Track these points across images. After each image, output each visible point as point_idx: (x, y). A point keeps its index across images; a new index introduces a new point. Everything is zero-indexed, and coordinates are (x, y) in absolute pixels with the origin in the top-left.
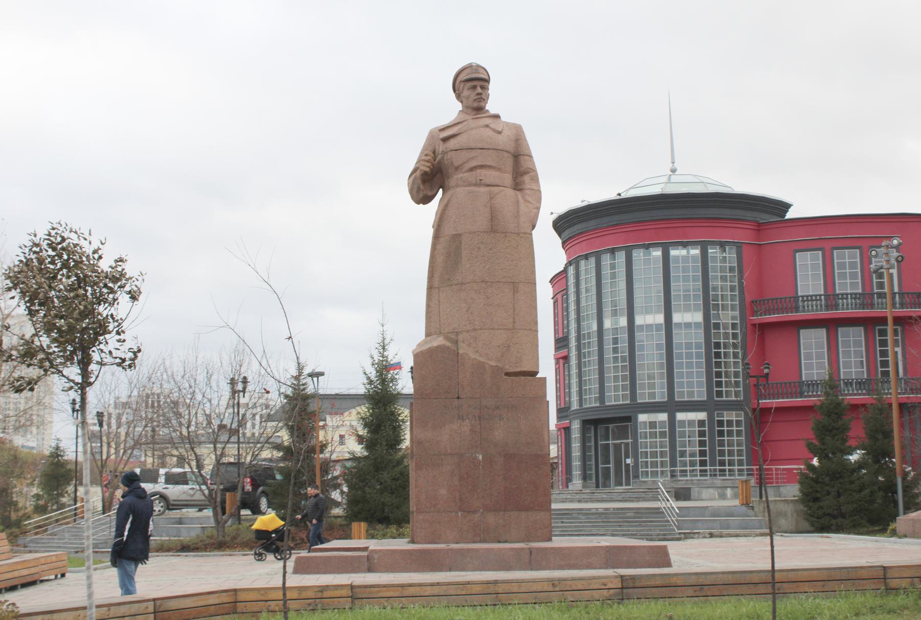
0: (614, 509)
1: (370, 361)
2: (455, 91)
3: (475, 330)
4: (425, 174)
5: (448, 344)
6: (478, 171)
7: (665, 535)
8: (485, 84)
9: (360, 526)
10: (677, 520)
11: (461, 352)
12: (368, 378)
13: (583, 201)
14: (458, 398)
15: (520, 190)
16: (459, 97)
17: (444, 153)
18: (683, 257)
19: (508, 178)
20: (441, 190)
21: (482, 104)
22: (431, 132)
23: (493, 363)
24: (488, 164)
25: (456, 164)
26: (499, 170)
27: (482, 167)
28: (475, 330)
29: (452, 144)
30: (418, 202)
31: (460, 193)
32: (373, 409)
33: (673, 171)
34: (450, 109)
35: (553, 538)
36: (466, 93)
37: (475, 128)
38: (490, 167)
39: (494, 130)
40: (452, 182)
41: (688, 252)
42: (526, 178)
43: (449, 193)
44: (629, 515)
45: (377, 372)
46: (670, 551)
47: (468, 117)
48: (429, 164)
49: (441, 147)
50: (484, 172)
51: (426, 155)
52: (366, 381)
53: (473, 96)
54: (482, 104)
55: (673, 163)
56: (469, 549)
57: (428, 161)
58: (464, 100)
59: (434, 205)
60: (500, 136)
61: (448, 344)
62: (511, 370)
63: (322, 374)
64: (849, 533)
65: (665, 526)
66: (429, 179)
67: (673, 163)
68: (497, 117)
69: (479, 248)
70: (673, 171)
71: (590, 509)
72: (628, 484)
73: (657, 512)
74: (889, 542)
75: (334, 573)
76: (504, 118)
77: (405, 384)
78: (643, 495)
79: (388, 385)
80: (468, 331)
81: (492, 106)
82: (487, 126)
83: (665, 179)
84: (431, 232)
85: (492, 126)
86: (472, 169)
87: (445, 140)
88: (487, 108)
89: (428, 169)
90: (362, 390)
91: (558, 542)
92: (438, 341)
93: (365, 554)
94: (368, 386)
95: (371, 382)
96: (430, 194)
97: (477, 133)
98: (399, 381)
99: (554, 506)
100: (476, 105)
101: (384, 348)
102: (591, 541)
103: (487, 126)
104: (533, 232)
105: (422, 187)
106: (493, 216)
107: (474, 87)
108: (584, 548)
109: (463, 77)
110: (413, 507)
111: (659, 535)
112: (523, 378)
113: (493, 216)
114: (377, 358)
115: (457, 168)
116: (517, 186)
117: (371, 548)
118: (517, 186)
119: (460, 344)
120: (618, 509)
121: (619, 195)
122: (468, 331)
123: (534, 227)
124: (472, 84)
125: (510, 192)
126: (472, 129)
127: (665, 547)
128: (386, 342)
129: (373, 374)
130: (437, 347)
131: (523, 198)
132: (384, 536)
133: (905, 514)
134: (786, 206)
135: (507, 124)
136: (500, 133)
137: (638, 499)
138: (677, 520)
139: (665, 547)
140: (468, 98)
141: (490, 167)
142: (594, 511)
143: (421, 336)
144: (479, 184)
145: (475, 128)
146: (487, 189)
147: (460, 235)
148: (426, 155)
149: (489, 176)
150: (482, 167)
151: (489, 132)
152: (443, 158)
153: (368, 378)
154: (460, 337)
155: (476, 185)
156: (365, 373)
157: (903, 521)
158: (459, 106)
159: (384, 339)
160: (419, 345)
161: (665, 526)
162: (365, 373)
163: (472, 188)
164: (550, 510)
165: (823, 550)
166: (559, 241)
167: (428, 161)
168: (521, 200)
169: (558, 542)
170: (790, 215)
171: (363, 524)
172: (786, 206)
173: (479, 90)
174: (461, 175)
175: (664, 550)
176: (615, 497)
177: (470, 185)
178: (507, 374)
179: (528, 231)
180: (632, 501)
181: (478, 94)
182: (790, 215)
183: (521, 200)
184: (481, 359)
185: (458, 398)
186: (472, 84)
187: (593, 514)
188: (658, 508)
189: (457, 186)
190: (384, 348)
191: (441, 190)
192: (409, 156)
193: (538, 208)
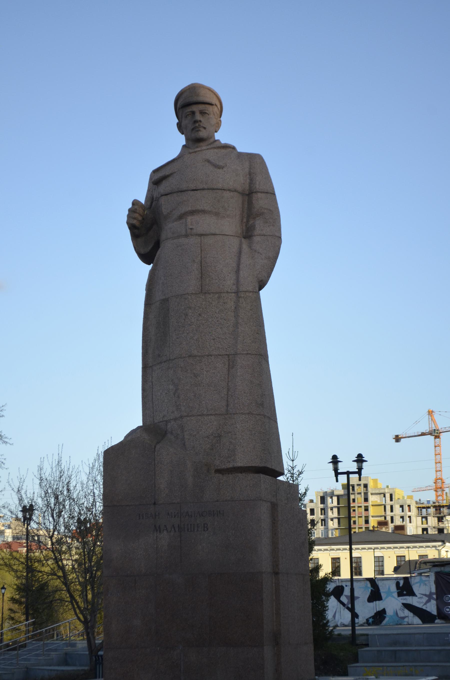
14: (155, 504)
26: (217, 214)
34: (172, 144)
86: (181, 217)
116: (248, 234)
124: (194, 110)
131: (250, 247)
178: (219, 471)
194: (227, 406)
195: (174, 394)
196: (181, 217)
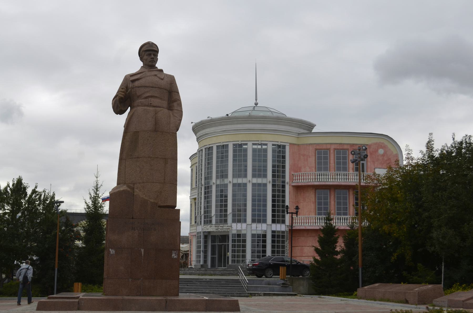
0: (215, 279)
1: (88, 196)
2: (139, 55)
3: (143, 182)
4: (121, 98)
5: (129, 189)
6: (150, 99)
7: (240, 294)
8: (156, 53)
9: (78, 285)
10: (247, 286)
11: (135, 194)
12: (88, 205)
13: (208, 117)
14: (133, 218)
15: (172, 110)
16: (141, 59)
17: (132, 88)
18: (259, 149)
19: (165, 104)
20: (129, 108)
21: (154, 64)
22: (126, 77)
23: (152, 201)
24: (155, 95)
25: (138, 94)
26: (161, 99)
27: (152, 97)
28: (143, 182)
29: (137, 83)
30: (117, 113)
31: (140, 109)
32: (89, 222)
33: (256, 104)
34: (136, 65)
35: (180, 294)
36: (145, 57)
37: (149, 76)
38: (156, 97)
39: (159, 78)
40: (135, 104)
41: (262, 147)
42: (175, 104)
43: (135, 109)
44: (222, 283)
45: (93, 202)
46: (240, 303)
47: (145, 70)
48: (123, 94)
49: (131, 85)
50: (152, 99)
51: (122, 89)
52: (86, 207)
53: (149, 59)
54: (154, 64)
55: (256, 100)
56: (133, 299)
57: (123, 92)
58: (144, 61)
59: (125, 115)
60: (162, 81)
61: (129, 189)
62: (162, 205)
63: (63, 202)
64: (329, 296)
65: (241, 289)
66: (120, 104)
67: (256, 100)
68: (161, 71)
69: (148, 139)
70: (256, 104)
71: (202, 279)
72: (225, 266)
73: (237, 281)
74: (353, 301)
75: (59, 310)
76: (165, 72)
77: (106, 208)
78: (232, 272)
79: (98, 210)
80: (140, 183)
81: (159, 65)
82: (156, 75)
83: (252, 109)
84: (123, 129)
85: (158, 75)
86: (146, 98)
87: (133, 81)
88: (156, 66)
89: (123, 96)
90: (84, 211)
91: (183, 296)
92: (124, 188)
93: (77, 300)
94: (87, 210)
95: (89, 207)
96: (123, 109)
97: (150, 79)
98: (104, 208)
99: (181, 277)
100: (150, 64)
101: (97, 190)
102: (199, 297)
103: (156, 75)
104: (177, 132)
105: (119, 105)
106: (156, 122)
107: (150, 55)
108: (194, 300)
109: (144, 49)
110: (105, 276)
111: (237, 294)
112: (167, 209)
113: (156, 122)
114: (93, 194)
115: (139, 97)
116: (170, 108)
117: (81, 297)
118: (170, 108)
119: (136, 190)
120: (217, 279)
121: (227, 115)
122: (140, 183)
123: (178, 130)
124: (149, 53)
125: (166, 111)
126: (147, 76)
127: (237, 301)
128: (99, 186)
129: (90, 203)
130: (123, 191)
131: (173, 114)
132: (92, 290)
133: (362, 286)
134: (313, 126)
135: (167, 75)
136: (162, 79)
137: (229, 274)
138: (247, 286)
139: (237, 301)
140: (146, 60)
141: (156, 97)
142: (204, 280)
143: (115, 184)
144: (150, 105)
145: (149, 76)
146: (154, 108)
147: (138, 132)
148: (122, 89)
149: (156, 102)
150: (152, 97)
151: (156, 79)
152: (131, 91)
153: (88, 205)
154: (136, 186)
155: (148, 106)
156: (86, 203)
157: (360, 291)
158: (141, 64)
159: (97, 185)
160: (113, 189)
161: (241, 289)
162: (86, 203)
163: (146, 108)
164: (178, 279)
165: (319, 304)
166: (195, 138)
167: (123, 92)
168: (172, 116)
169: (183, 296)
170: (314, 131)
171: (80, 284)
172: (313, 126)
173: (153, 56)
174: (140, 101)
175: (236, 302)
176: (217, 272)
177: (145, 106)
178: (160, 207)
179: (174, 132)
180: (226, 275)
181: (152, 58)
182: (314, 130)
183: (172, 116)
184: (146, 198)
185: (133, 218)
186: (149, 53)
187: (204, 282)
188: (239, 280)
189: (138, 106)
190: (97, 190)
191: (129, 108)
192: (113, 88)
193: (181, 120)
194: (165, 180)
195: (140, 172)
196: (146, 98)
